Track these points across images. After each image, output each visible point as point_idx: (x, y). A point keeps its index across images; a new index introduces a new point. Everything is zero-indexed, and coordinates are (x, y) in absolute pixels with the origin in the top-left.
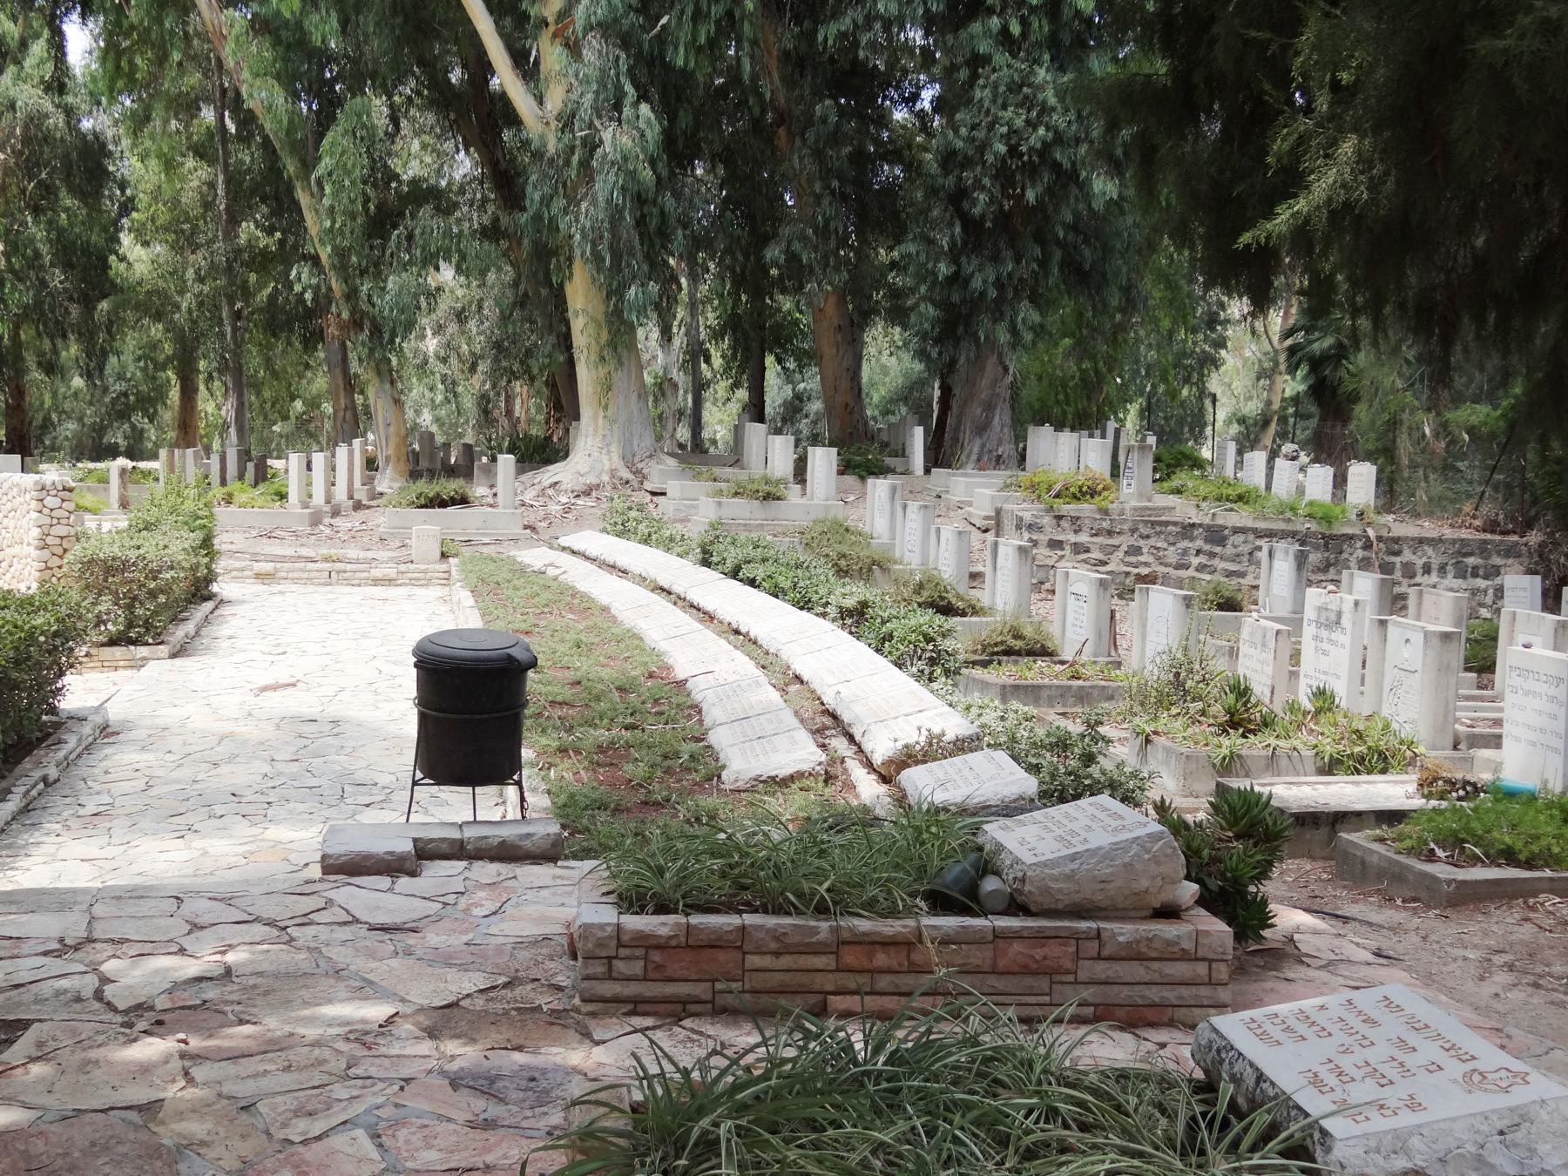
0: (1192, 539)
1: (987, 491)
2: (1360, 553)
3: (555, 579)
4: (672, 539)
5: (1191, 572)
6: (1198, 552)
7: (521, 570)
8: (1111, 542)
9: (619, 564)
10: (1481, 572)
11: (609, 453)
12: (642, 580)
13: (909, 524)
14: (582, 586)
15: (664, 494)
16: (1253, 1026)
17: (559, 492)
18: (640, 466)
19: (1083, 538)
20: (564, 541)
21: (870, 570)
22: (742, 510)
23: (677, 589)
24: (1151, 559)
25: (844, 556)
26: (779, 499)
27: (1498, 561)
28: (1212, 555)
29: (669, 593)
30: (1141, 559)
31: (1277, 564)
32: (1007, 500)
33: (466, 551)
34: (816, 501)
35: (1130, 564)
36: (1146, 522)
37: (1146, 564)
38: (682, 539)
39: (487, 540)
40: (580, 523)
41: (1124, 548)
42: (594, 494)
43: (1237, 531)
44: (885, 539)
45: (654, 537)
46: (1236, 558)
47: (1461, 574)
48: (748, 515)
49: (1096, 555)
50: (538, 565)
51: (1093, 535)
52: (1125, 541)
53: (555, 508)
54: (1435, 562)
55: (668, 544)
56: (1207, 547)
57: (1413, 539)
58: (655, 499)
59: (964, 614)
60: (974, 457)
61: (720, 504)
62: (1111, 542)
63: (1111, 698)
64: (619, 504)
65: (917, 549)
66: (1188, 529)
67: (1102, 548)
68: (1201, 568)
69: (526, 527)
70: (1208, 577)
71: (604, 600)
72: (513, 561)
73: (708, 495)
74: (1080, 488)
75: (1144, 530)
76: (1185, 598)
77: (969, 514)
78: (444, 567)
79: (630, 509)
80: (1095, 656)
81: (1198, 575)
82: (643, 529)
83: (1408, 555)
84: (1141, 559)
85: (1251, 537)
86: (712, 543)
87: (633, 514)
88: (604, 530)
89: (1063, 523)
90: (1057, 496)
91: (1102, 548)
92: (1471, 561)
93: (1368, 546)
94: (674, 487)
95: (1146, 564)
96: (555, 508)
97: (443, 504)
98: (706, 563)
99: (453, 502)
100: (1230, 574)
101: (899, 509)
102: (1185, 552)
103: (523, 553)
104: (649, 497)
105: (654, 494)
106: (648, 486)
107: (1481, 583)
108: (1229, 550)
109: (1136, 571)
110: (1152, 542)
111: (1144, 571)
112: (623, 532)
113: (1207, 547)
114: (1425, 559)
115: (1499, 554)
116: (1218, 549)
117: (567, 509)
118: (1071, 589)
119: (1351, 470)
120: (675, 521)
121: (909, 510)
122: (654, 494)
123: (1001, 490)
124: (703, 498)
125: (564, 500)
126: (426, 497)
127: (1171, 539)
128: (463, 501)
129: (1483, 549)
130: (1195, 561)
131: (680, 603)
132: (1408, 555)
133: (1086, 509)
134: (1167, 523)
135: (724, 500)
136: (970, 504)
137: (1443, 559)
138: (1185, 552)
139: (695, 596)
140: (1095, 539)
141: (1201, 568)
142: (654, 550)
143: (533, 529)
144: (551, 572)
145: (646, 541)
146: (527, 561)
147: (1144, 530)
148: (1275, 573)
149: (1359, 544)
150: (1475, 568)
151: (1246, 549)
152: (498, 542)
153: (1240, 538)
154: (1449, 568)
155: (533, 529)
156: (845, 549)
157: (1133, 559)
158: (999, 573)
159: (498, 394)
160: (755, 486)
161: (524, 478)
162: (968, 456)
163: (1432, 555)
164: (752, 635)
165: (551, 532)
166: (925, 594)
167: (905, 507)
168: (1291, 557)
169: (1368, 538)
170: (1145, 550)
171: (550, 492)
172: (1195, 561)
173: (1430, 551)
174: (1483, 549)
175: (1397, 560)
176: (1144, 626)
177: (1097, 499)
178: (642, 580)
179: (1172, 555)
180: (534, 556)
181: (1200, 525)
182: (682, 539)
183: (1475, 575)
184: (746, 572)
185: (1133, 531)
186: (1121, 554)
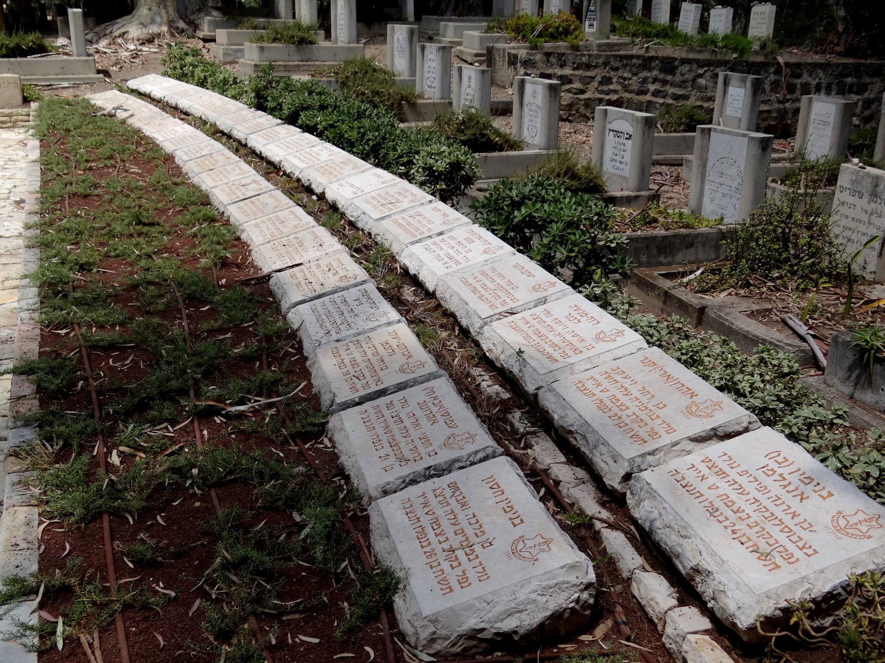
0: (650, 70)
1: (476, 33)
2: (772, 77)
3: (123, 122)
4: (225, 81)
5: (648, 97)
6: (655, 80)
7: (91, 113)
8: (588, 74)
9: (181, 106)
10: (855, 89)
11: (165, 7)
12: (201, 124)
13: (427, 64)
14: (149, 131)
15: (214, 40)
16: (580, 385)
17: (126, 41)
18: (192, 17)
19: (567, 71)
20: (133, 84)
21: (400, 105)
22: (281, 52)
23: (239, 134)
24: (619, 88)
25: (378, 93)
26: (311, 43)
27: (867, 80)
28: (665, 82)
29: (229, 137)
30: (612, 87)
31: (731, 90)
32: (498, 40)
33: (46, 95)
34: (340, 44)
35: (602, 92)
36: (616, 56)
37: (615, 92)
38: (235, 83)
39: (66, 84)
40: (146, 68)
41: (599, 78)
42: (156, 41)
43: (684, 61)
44: (406, 77)
45: (209, 80)
46: (682, 84)
47: (841, 92)
48: (286, 58)
49: (576, 85)
50: (109, 107)
51: (574, 69)
52: (598, 74)
53: (124, 54)
54: (824, 82)
55: (223, 87)
56: (661, 76)
57: (810, 64)
58: (207, 45)
59: (501, 149)
60: (452, 6)
61: (262, 49)
62: (588, 74)
63: (691, 245)
64: (176, 51)
65: (437, 84)
66: (647, 62)
67: (582, 79)
68: (656, 93)
69: (99, 72)
70: (661, 101)
71: (168, 147)
72: (87, 104)
73: (251, 41)
74: (557, 28)
75: (615, 64)
76: (762, 140)
77: (461, 52)
78: (25, 110)
79: (187, 54)
80: (639, 190)
81: (654, 99)
82: (198, 72)
83: (806, 78)
84: (612, 87)
85: (695, 66)
86: (266, 88)
87: (189, 59)
88: (165, 74)
89: (553, 60)
90: (540, 35)
91: (582, 79)
92: (849, 80)
93: (778, 71)
94: (222, 34)
95: (615, 92)
96: (124, 54)
97: (24, 53)
98: (260, 106)
99: (31, 51)
100: (677, 97)
101: (418, 50)
102: (645, 81)
103: (97, 96)
104: (202, 43)
105: (205, 40)
106: (201, 34)
107: (855, 98)
108: (678, 78)
109: (607, 97)
110: (620, 73)
111: (614, 97)
112: (182, 77)
113: (661, 76)
114: (817, 80)
115: (868, 74)
116: (669, 78)
117: (135, 56)
118: (609, 126)
119: (754, 10)
120: (225, 63)
121: (427, 52)
122: (205, 40)
123: (486, 32)
124: (247, 44)
125: (132, 47)
126: (7, 48)
127: (635, 70)
128: (41, 50)
129: (857, 71)
130: (652, 88)
131: (243, 151)
132: (806, 78)
133: (562, 45)
134: (631, 57)
135: (265, 45)
136: (459, 44)
137: (829, 80)
138: (645, 81)
139: (256, 142)
140: (577, 72)
141: (656, 93)
142: (209, 92)
143: (106, 73)
144: (121, 115)
145: (202, 84)
146: (99, 103)
147: (615, 64)
148: (729, 99)
149: (772, 70)
150: (852, 85)
151: (690, 76)
152: (76, 86)
153: (685, 68)
154: (834, 86)
155: (106, 73)
156: (377, 87)
157: (605, 88)
158: (526, 109)
159: (652, 648)
160: (291, 33)
161: (509, 100)
162: (448, 5)
163: (822, 76)
164: (330, 196)
165: (122, 76)
166: (469, 132)
167: (423, 49)
168: (749, 84)
169: (778, 64)
170: (614, 80)
171: (120, 41)
172: (652, 88)
173: (821, 74)
174: (857, 71)
175: (798, 81)
176: (704, 166)
177: (570, 37)
178: (201, 124)
179: (635, 83)
180: (106, 99)
181: (657, 58)
182: (235, 83)
183: (850, 92)
184: (303, 117)
185: (606, 64)
186: (595, 84)
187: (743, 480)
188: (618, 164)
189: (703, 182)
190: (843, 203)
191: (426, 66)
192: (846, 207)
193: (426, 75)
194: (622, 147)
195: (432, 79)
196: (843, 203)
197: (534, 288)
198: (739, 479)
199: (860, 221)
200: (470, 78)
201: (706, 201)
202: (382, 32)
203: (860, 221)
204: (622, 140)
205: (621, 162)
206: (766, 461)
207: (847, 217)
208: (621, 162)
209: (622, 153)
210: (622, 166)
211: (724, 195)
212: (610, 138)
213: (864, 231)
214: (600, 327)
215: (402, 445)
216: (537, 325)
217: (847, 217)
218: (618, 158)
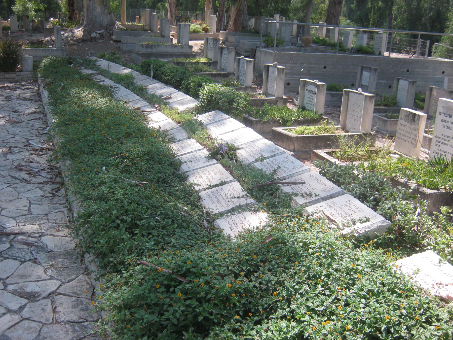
187: (337, 209)
188: (310, 105)
189: (346, 115)
190: (402, 125)
191: (223, 56)
192: (403, 126)
193: (223, 61)
194: (312, 98)
195: (225, 63)
196: (402, 125)
197: (270, 151)
198: (337, 208)
199: (408, 132)
200: (243, 63)
201: (347, 122)
202: (390, 128)
203: (408, 132)
204: (312, 95)
205: (311, 104)
206: (346, 203)
207: (403, 131)
208: (311, 104)
209: (312, 100)
210: (311, 106)
211: (355, 120)
212: (307, 94)
213: (410, 136)
214: (295, 165)
215: (222, 202)
216: (271, 164)
217: (403, 131)
218: (310, 102)
